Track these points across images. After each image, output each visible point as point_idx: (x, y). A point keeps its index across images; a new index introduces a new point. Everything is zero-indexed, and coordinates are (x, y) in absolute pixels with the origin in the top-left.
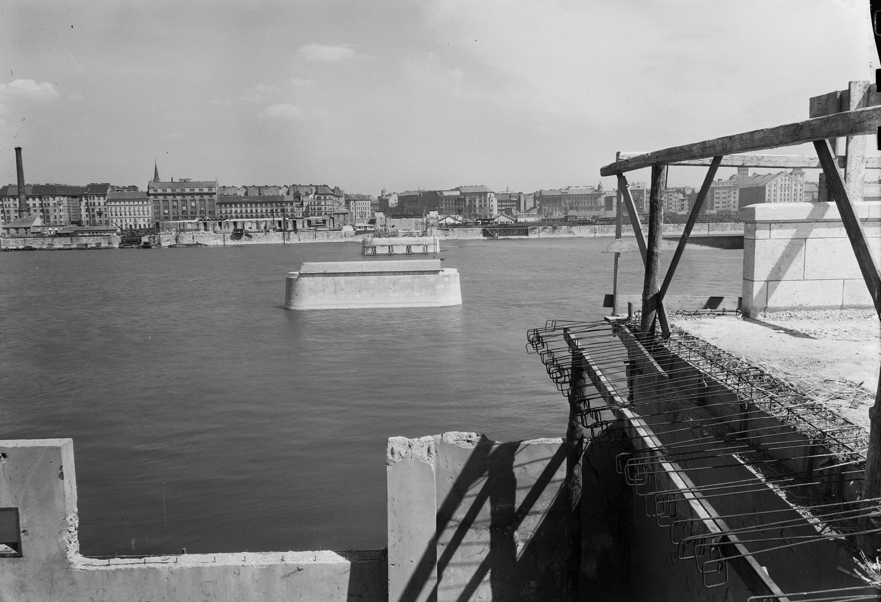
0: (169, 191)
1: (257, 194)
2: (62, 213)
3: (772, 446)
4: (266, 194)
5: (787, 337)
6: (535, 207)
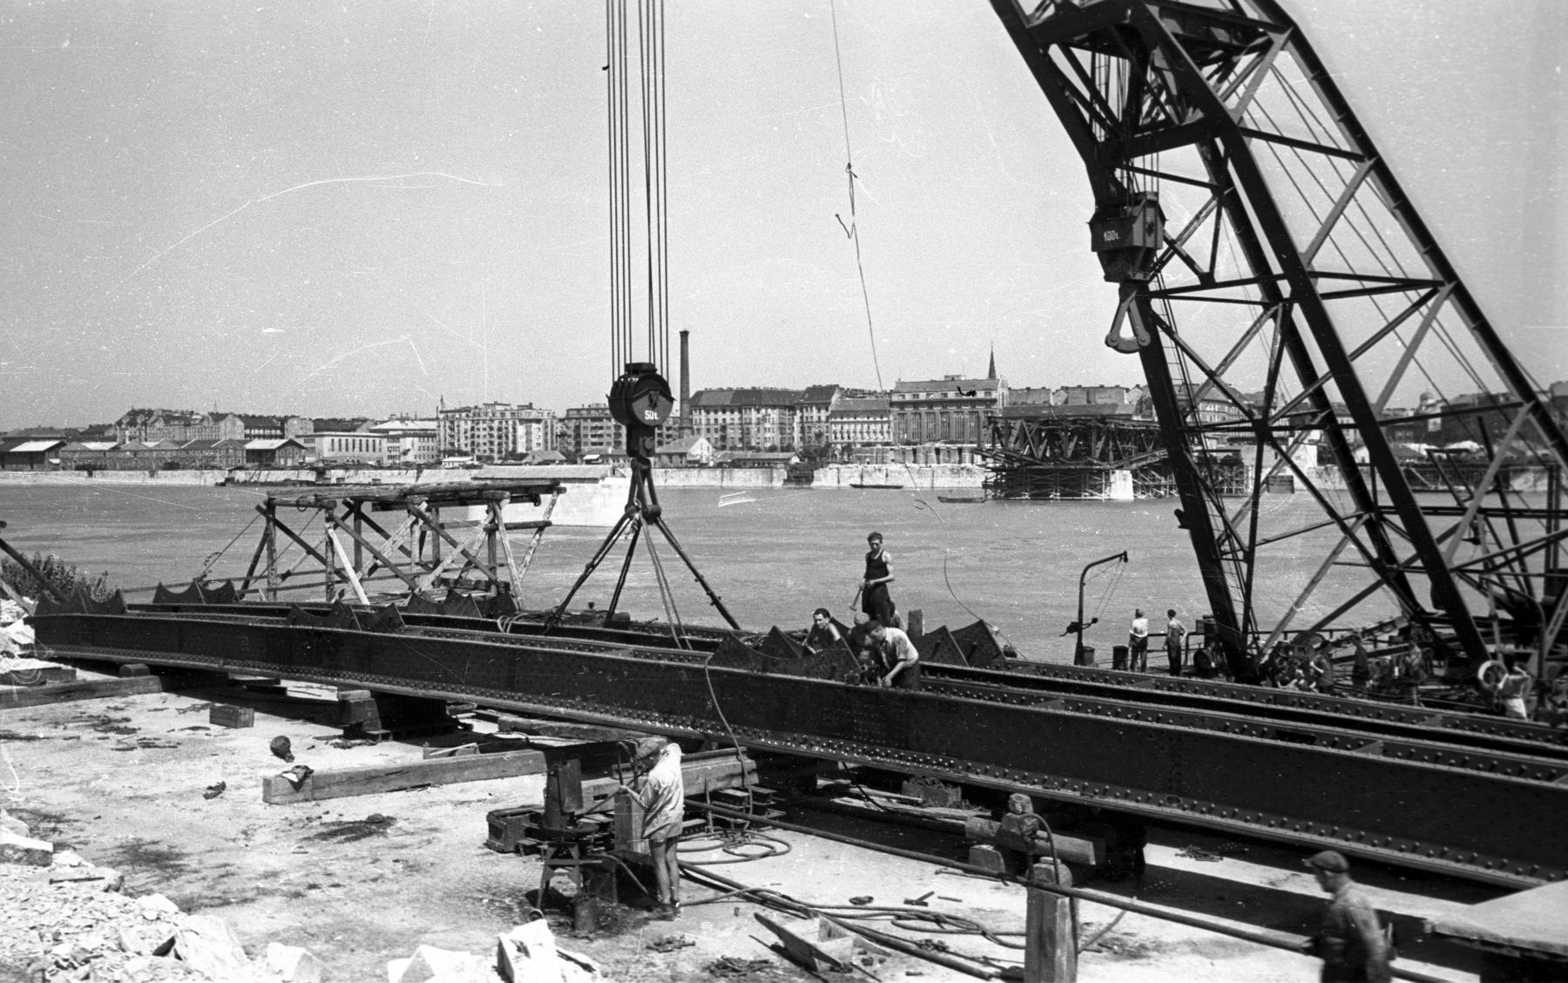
0: (923, 396)
1: (1084, 402)
2: (768, 435)
3: (235, 672)
4: (1100, 401)
5: (580, 969)
6: (1451, 491)
